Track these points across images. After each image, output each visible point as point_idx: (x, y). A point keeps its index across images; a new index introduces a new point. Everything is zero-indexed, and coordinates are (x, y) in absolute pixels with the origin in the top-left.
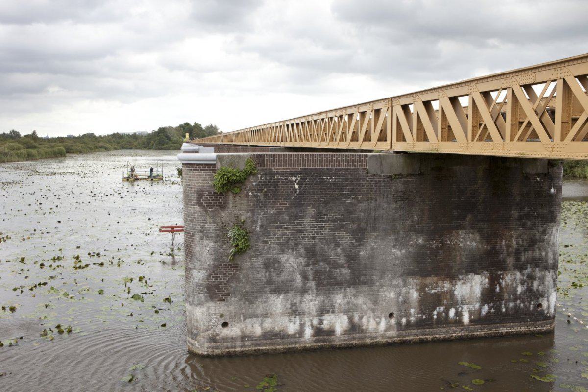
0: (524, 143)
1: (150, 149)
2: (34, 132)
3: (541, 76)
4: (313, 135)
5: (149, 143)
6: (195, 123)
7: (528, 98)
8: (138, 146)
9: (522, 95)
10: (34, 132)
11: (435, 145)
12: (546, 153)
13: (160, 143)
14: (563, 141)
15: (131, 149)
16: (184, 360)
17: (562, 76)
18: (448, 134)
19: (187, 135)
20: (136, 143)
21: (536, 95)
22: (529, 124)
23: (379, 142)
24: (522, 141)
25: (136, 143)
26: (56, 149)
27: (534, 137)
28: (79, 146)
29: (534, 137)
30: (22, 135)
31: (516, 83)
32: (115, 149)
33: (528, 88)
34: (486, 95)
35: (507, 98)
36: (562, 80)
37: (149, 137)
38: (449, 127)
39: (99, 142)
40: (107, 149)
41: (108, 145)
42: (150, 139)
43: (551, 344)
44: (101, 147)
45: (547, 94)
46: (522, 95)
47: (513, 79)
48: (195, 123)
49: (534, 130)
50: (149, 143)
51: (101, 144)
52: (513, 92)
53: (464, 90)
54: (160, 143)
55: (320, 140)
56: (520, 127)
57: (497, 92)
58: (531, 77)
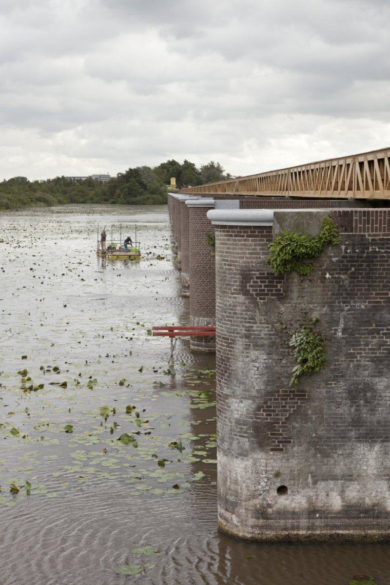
1: (113, 203)
2: (5, 180)
5: (112, 194)
6: (186, 162)
8: (96, 199)
10: (5, 180)
13: (130, 194)
15: (84, 202)
19: (173, 181)
20: (92, 193)
25: (92, 193)
32: (60, 203)
40: (49, 204)
41: (49, 197)
48: (186, 162)
50: (112, 194)
51: (39, 194)
54: (130, 194)
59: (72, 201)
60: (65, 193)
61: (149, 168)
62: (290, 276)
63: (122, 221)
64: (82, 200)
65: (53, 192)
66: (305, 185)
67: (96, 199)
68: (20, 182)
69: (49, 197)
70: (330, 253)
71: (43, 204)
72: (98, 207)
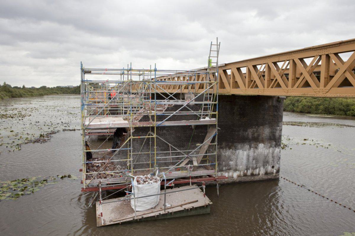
0: (253, 89)
3: (282, 58)
4: (164, 86)
5: (75, 91)
7: (276, 69)
8: (70, 92)
9: (272, 66)
11: (230, 91)
12: (242, 93)
14: (325, 87)
15: (67, 93)
16: (136, 126)
17: (293, 58)
18: (236, 85)
20: (69, 91)
21: (279, 68)
22: (276, 80)
23: (199, 89)
24: (252, 88)
25: (69, 91)
26: (40, 93)
27: (279, 86)
28: (36, 92)
29: (279, 86)
30: (12, 86)
31: (270, 62)
32: (60, 93)
33: (275, 64)
34: (255, 67)
35: (290, 63)
36: (292, 61)
37: (75, 89)
38: (223, 82)
39: (53, 90)
40: (58, 94)
41: (57, 92)
42: (76, 89)
43: (277, 185)
44: (55, 93)
45: (284, 68)
46: (298, 62)
47: (269, 59)
49: (256, 84)
50: (75, 91)
51: (54, 91)
52: (268, 65)
53: (245, 64)
55: (167, 89)
56: (272, 82)
57: (260, 66)
58: (277, 58)
59: (64, 93)
60: (61, 91)
61: (10, 86)
62: (227, 153)
63: (287, 122)
64: (66, 93)
65: (58, 91)
66: (97, 87)
67: (70, 92)
68: (44, 88)
69: (57, 92)
70: (245, 134)
71: (56, 94)
72: (72, 95)
